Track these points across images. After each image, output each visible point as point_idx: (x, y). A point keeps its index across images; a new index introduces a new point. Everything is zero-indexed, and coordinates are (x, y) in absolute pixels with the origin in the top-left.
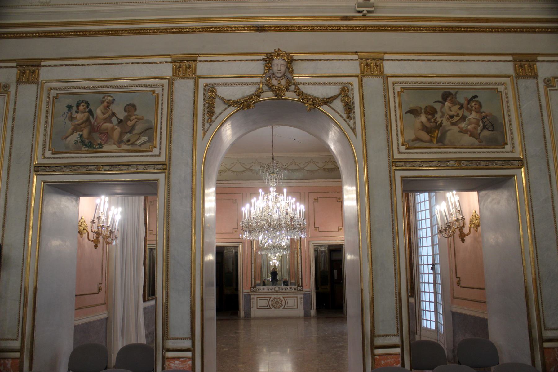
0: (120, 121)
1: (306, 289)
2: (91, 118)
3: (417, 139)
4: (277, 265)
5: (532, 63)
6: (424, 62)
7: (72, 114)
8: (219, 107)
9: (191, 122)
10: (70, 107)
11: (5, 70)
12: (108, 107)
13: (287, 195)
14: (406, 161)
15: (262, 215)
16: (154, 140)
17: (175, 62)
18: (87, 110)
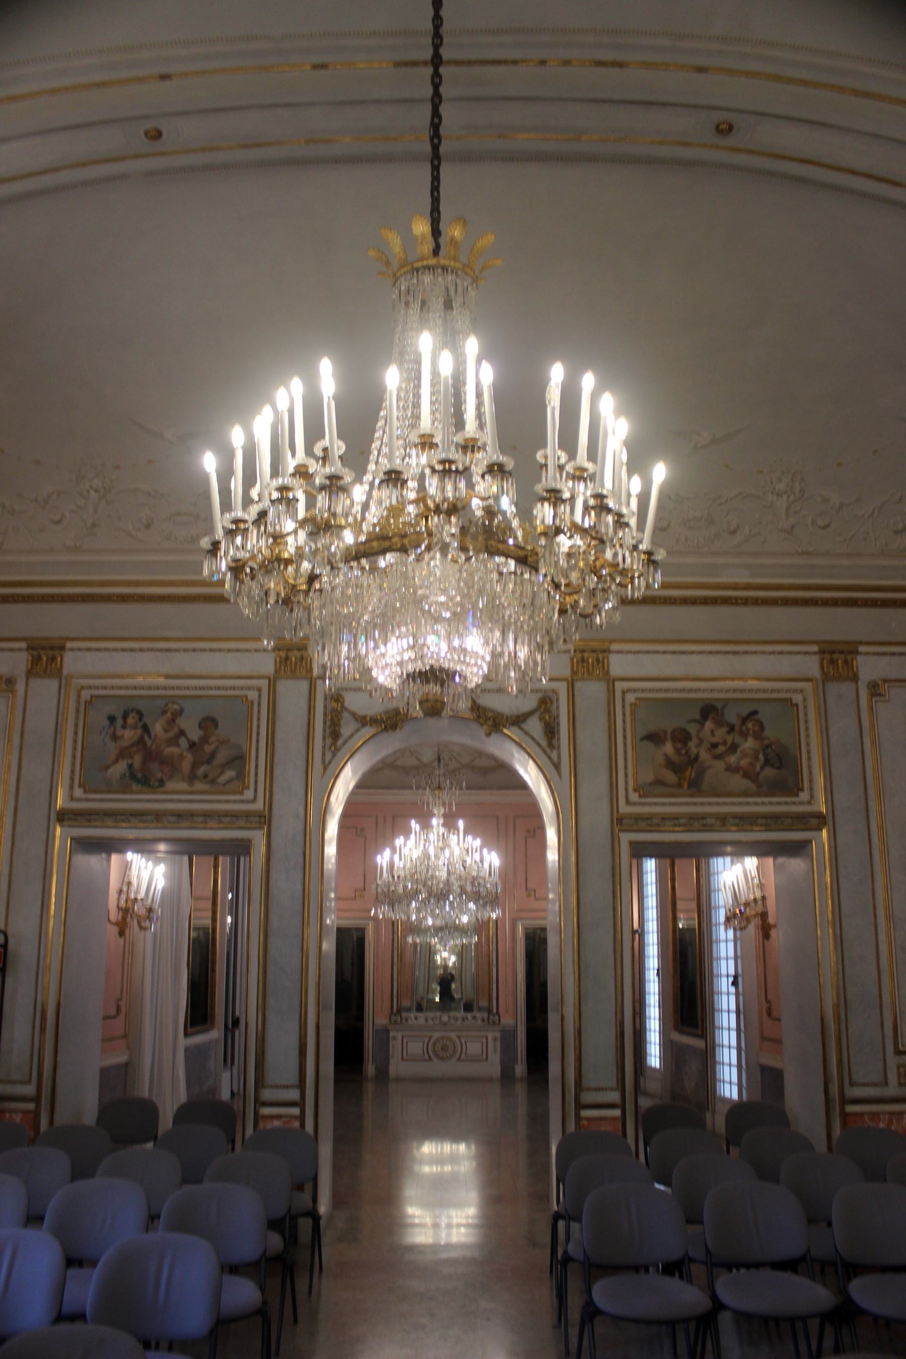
0: (192, 745)
1: (507, 1020)
2: (146, 737)
3: (659, 782)
4: (450, 964)
5: (849, 657)
6: (675, 656)
7: (115, 730)
8: (346, 729)
9: (303, 750)
10: (112, 719)
11: (8, 654)
12: (173, 720)
13: (466, 833)
14: (637, 818)
15: (416, 872)
16: (245, 776)
17: (279, 650)
18: (140, 724)
